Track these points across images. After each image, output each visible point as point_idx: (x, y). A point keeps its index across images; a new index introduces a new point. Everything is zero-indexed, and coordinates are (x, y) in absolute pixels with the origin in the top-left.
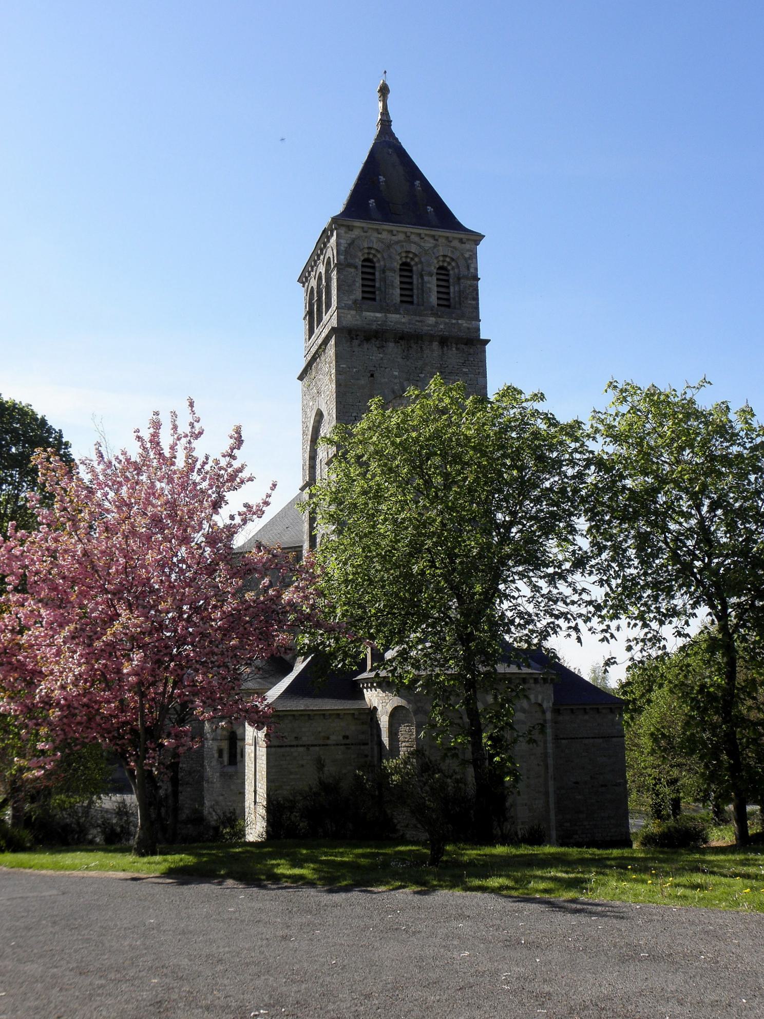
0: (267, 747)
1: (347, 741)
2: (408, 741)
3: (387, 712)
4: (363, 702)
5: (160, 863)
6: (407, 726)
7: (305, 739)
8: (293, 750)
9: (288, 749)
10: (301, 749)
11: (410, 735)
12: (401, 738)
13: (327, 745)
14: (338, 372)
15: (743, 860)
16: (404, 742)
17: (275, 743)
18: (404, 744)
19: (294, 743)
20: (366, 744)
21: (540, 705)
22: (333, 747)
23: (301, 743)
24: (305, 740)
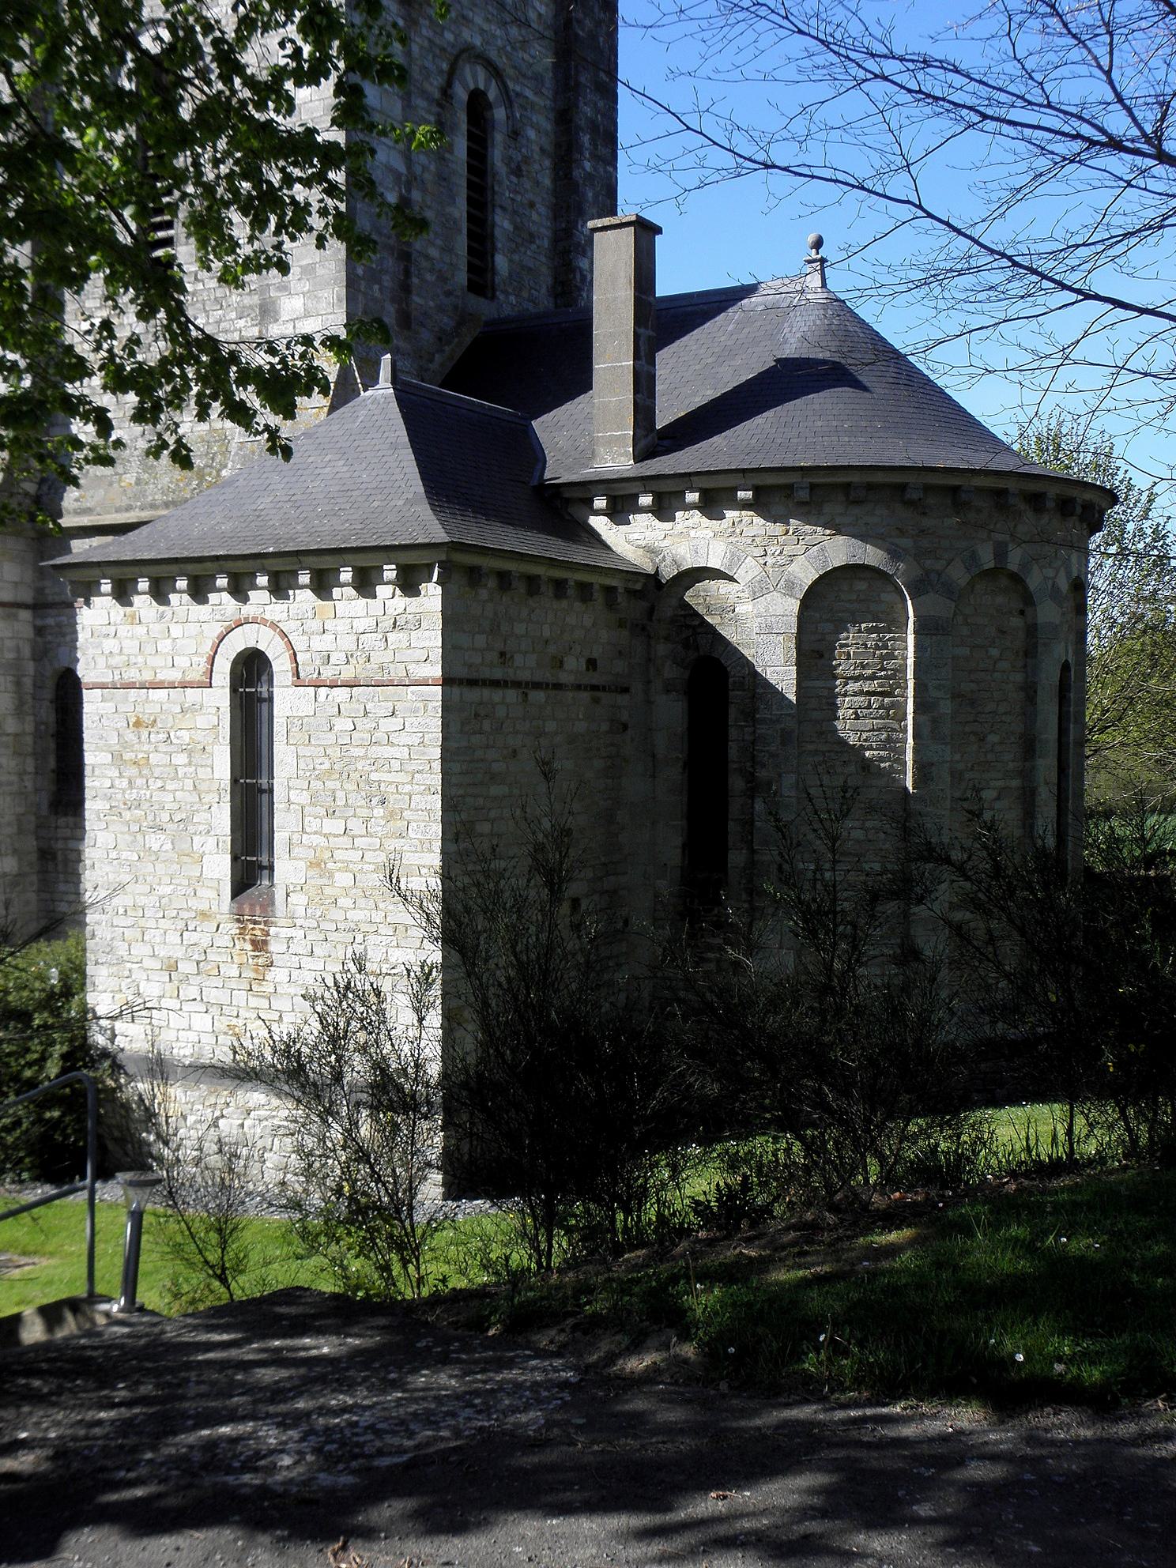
0: (447, 681)
1: (596, 679)
2: (873, 678)
3: (790, 586)
4: (1077, 532)
5: (863, 1465)
6: (870, 631)
7: (519, 660)
8: (497, 695)
9: (486, 693)
10: (512, 695)
11: (883, 658)
12: (844, 667)
13: (558, 686)
14: (352, 283)
15: (565, 1490)
16: (856, 679)
17: (461, 672)
18: (853, 686)
19: (498, 674)
20: (626, 690)
21: (1017, 579)
22: (570, 694)
23: (510, 674)
24: (526, 666)
